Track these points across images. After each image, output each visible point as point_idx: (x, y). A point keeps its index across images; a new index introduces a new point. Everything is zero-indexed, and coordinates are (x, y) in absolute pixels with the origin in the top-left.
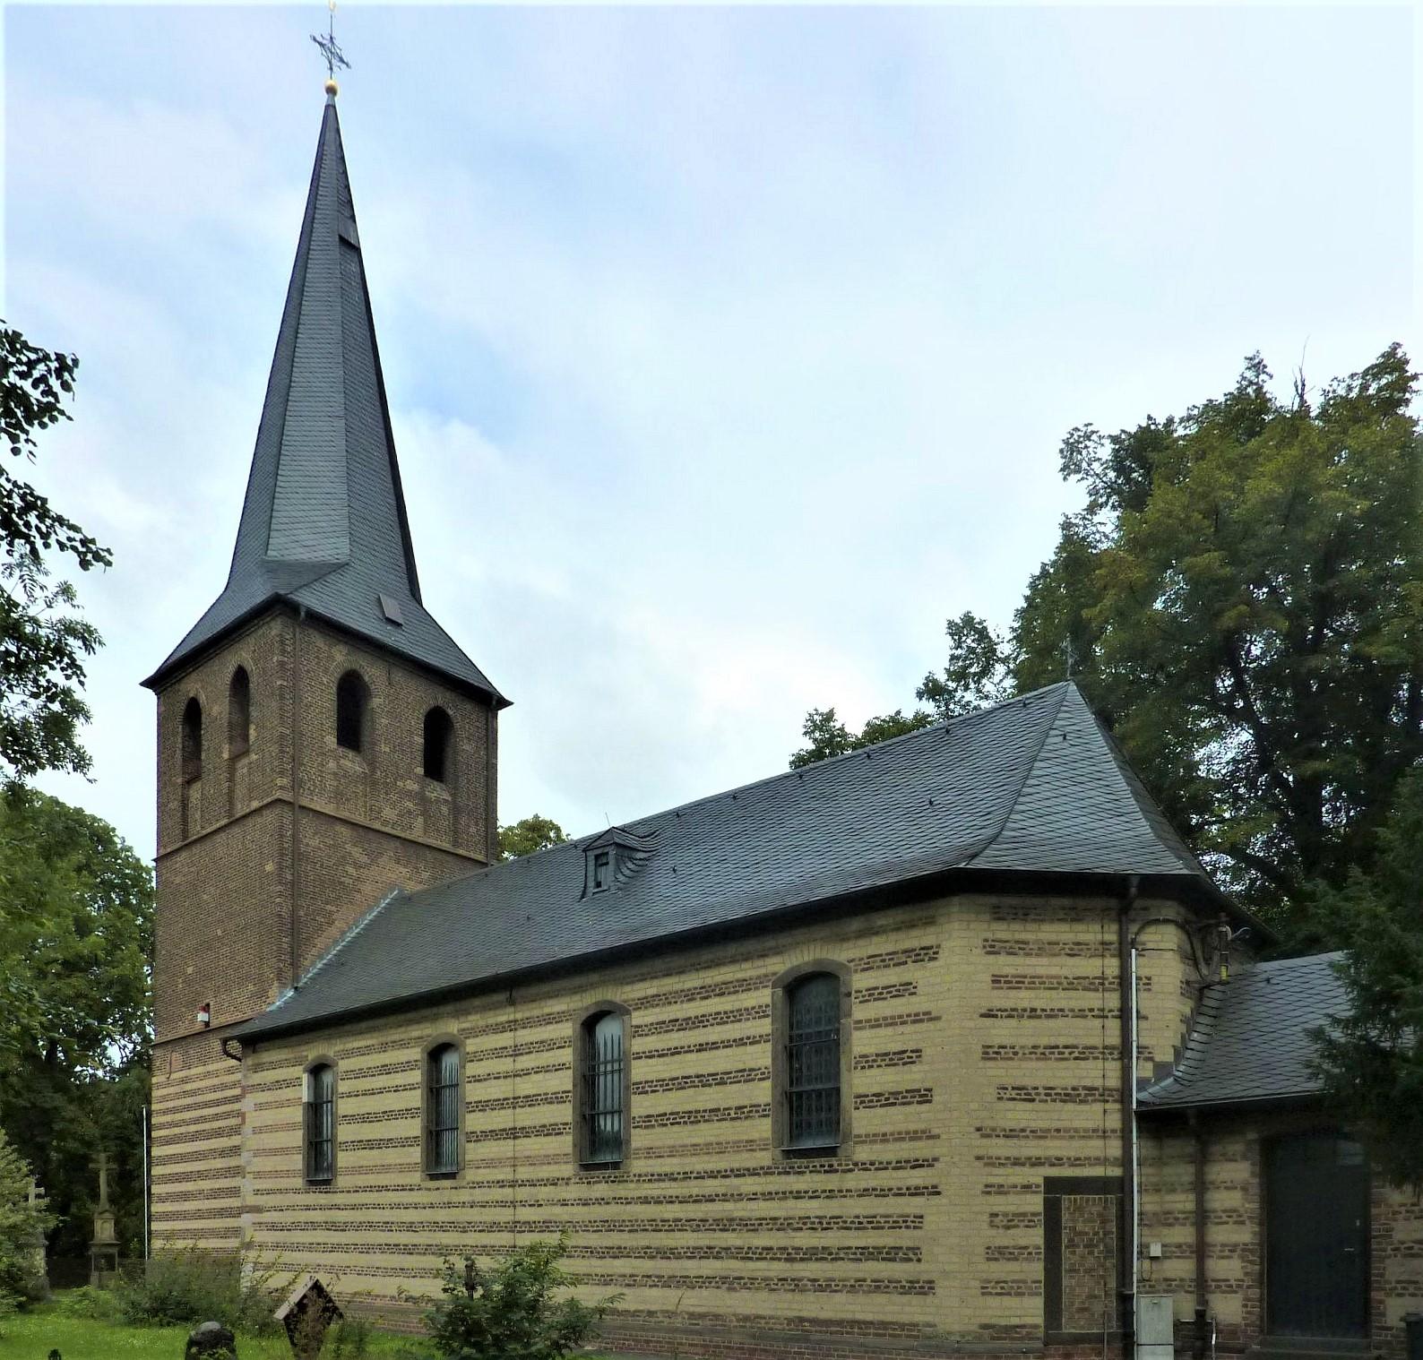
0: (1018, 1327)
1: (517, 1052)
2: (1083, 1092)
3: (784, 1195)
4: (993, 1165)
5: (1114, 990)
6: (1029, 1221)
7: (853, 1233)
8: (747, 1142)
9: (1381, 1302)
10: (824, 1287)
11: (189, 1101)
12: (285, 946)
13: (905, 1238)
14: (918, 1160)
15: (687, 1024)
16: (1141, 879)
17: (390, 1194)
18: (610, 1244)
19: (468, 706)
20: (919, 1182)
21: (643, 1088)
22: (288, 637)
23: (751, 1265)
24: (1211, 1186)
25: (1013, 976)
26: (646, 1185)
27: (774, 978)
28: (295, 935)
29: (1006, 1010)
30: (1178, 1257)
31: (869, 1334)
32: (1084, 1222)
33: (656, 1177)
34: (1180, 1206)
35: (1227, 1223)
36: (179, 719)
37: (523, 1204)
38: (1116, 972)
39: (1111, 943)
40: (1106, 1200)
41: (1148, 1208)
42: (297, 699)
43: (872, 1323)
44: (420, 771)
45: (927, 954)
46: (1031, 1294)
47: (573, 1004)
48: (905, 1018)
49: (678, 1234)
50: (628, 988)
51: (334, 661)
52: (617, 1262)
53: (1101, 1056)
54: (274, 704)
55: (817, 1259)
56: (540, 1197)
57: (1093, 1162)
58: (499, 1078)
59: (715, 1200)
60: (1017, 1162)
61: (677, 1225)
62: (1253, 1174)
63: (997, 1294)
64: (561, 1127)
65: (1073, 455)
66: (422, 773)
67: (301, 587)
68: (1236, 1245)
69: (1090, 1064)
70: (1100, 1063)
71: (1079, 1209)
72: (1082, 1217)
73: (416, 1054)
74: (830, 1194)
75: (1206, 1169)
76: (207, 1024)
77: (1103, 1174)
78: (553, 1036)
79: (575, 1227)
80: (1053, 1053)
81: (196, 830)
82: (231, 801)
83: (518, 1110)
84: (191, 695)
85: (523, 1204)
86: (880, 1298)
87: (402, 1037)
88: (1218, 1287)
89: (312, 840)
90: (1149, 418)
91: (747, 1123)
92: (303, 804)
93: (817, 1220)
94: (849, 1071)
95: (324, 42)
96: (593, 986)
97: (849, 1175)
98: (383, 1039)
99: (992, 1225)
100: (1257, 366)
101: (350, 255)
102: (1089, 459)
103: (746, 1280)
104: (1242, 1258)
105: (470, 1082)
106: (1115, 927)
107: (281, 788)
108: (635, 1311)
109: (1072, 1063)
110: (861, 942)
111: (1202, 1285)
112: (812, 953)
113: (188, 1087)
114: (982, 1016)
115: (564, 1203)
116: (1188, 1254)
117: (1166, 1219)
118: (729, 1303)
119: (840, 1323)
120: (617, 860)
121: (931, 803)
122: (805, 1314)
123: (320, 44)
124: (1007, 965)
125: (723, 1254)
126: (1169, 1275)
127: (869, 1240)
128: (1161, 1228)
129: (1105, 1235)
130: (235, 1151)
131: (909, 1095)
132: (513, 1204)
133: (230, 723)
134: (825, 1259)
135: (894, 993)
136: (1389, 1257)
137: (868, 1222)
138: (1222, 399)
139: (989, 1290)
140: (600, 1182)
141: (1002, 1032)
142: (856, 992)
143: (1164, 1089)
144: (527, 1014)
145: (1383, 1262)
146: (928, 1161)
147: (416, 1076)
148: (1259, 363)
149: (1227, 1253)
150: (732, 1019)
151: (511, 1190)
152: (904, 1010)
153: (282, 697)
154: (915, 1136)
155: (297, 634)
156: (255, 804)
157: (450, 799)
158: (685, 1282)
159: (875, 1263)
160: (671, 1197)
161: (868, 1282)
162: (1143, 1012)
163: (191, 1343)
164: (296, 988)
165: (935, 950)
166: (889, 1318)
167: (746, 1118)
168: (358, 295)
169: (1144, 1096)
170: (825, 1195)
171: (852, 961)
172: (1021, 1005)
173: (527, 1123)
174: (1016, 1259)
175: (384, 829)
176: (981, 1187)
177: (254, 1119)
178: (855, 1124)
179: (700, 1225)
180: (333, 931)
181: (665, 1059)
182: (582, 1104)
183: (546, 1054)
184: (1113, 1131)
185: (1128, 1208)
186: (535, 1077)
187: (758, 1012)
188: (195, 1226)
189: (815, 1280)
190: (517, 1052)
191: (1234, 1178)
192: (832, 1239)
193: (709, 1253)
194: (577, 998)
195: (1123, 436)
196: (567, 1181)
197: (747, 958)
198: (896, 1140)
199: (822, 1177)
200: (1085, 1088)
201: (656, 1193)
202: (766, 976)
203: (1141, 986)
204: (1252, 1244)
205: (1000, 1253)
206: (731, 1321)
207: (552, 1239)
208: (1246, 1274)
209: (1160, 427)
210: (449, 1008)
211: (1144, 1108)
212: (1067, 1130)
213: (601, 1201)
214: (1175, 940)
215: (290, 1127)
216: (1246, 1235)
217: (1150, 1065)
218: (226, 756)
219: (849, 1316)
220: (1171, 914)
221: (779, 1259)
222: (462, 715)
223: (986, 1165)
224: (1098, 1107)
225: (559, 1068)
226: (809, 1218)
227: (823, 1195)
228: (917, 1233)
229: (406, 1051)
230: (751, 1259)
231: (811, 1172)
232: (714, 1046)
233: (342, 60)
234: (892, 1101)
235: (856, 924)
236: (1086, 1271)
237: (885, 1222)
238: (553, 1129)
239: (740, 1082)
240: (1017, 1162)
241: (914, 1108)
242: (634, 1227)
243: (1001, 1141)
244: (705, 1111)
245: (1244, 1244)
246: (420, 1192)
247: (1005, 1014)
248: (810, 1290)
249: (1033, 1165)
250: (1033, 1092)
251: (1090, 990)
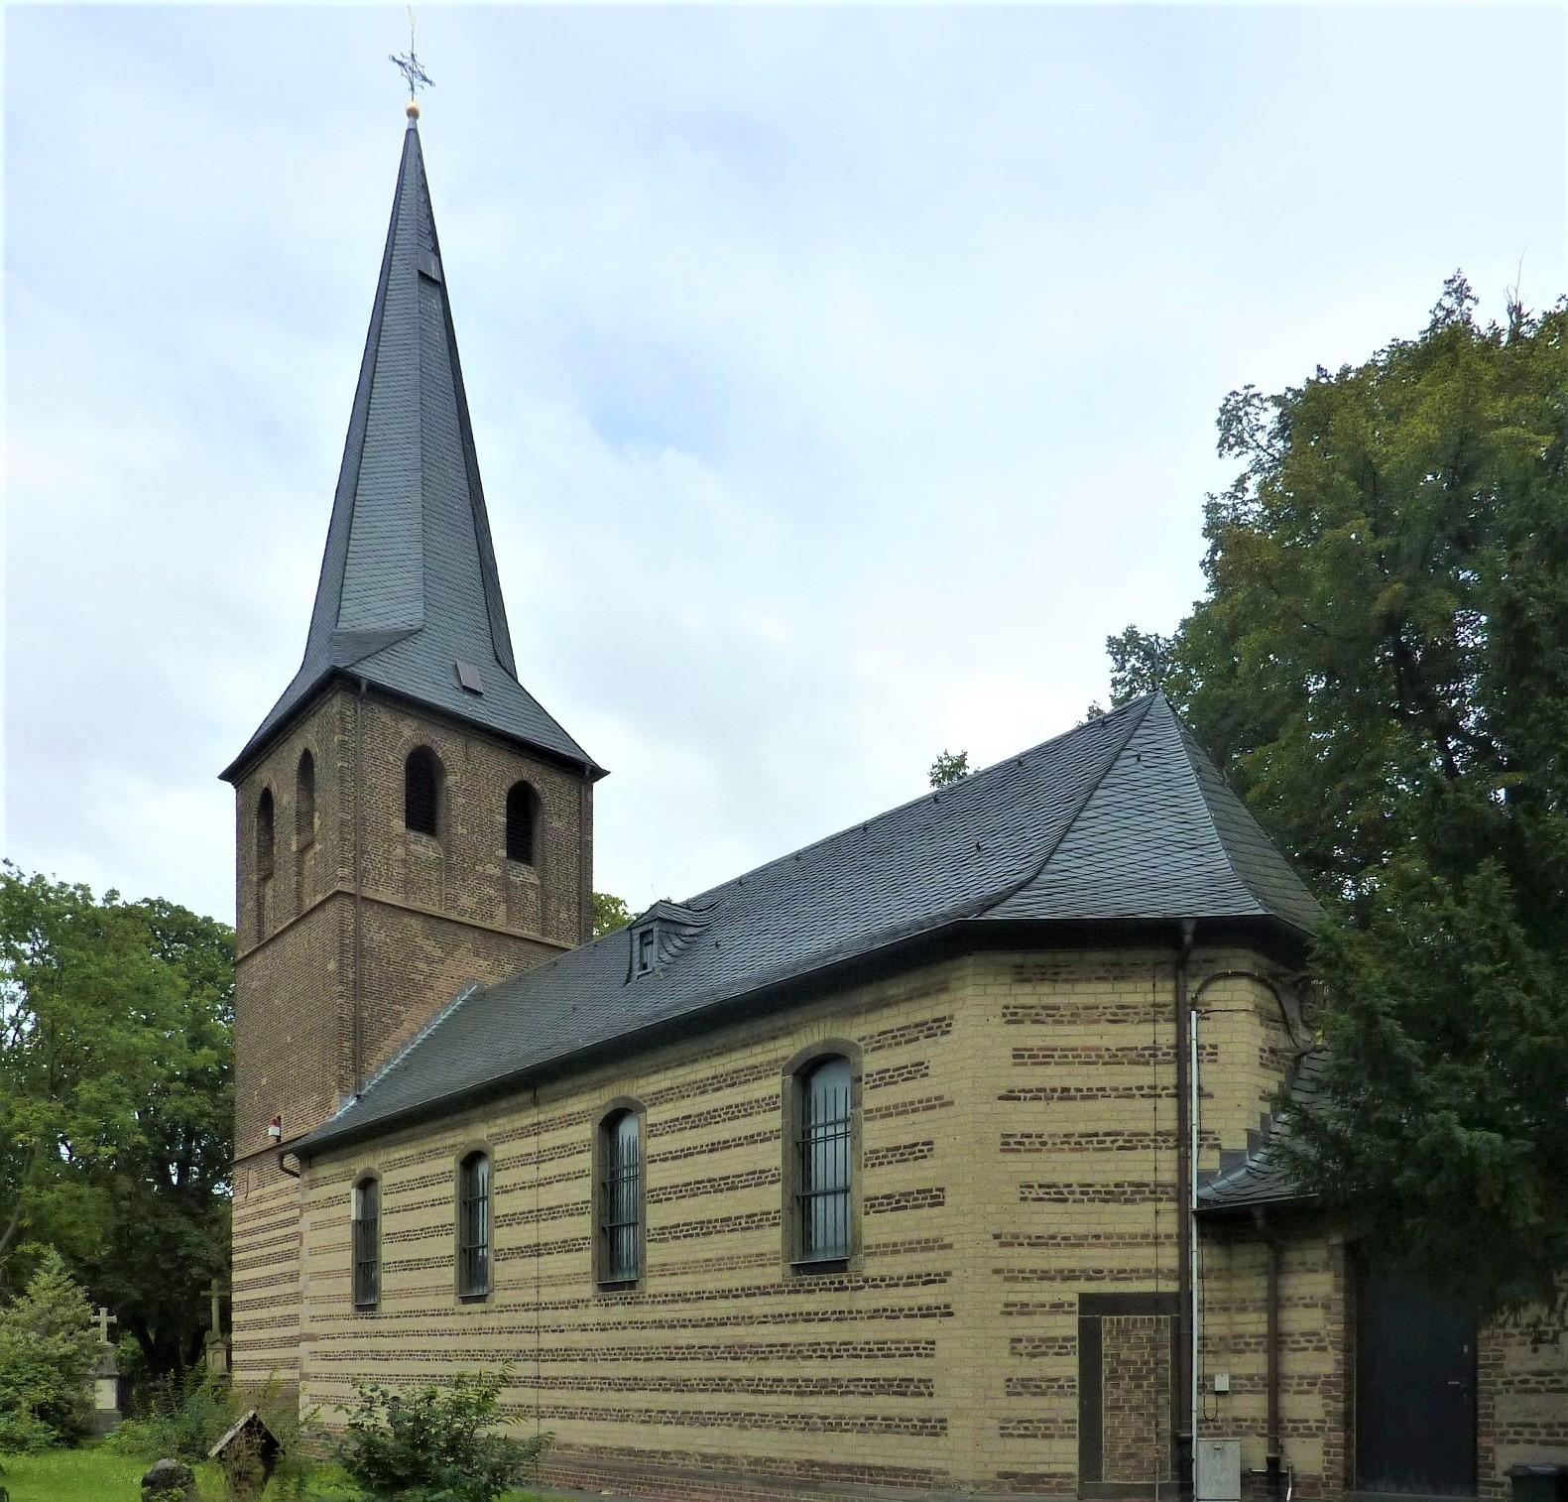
0: (1045, 1475)
1: (540, 1158)
2: (1129, 1190)
3: (794, 1318)
4: (1014, 1279)
5: (1169, 1062)
6: (1061, 1347)
7: (863, 1362)
8: (757, 1255)
9: (1490, 1450)
10: (834, 1425)
11: (263, 1221)
12: (346, 1051)
13: (912, 1368)
14: (929, 1275)
15: (700, 1120)
16: (1197, 925)
17: (428, 1319)
18: (626, 1375)
19: (558, 779)
20: (931, 1301)
21: (658, 1195)
22: (348, 713)
23: (762, 1399)
24: (1287, 1304)
25: (1041, 1049)
26: (661, 1307)
27: (784, 1063)
28: (357, 1042)
29: (1031, 1091)
30: (1251, 1392)
31: (879, 1482)
32: (1129, 1349)
33: (670, 1298)
34: (1252, 1329)
35: (1305, 1349)
36: (255, 812)
37: (547, 1329)
38: (1172, 1040)
39: (1165, 1005)
40: (1158, 1320)
41: (1211, 1331)
42: (360, 781)
43: (882, 1469)
44: (503, 853)
45: (938, 1027)
46: (1062, 1437)
47: (591, 1101)
48: (917, 1105)
49: (690, 1363)
50: (643, 1082)
51: (402, 736)
52: (634, 1395)
53: (1152, 1145)
54: (335, 787)
55: (827, 1393)
56: (562, 1321)
57: (1142, 1274)
58: (524, 1188)
59: (726, 1324)
60: (1045, 1276)
61: (689, 1353)
62: (1336, 1289)
63: (1019, 1436)
64: (581, 1242)
65: (1231, 423)
66: (505, 854)
67: (364, 659)
68: (1316, 1377)
69: (1139, 1154)
70: (1150, 1154)
71: (1124, 1332)
72: (1130, 1344)
73: (449, 1164)
74: (840, 1316)
75: (1281, 1282)
76: (278, 1138)
77: (1153, 1290)
78: (574, 1139)
79: (593, 1355)
80: (1091, 1142)
81: (270, 931)
82: (299, 898)
83: (542, 1224)
84: (265, 785)
85: (547, 1329)
86: (891, 1439)
87: (439, 1145)
88: (1296, 1429)
89: (377, 933)
90: (1319, 369)
91: (758, 1233)
92: (367, 895)
93: (827, 1347)
94: (859, 1169)
95: (404, 61)
96: (610, 1081)
97: (860, 1293)
98: (421, 1149)
99: (1014, 1352)
100: (1459, 290)
101: (431, 291)
102: (1251, 428)
103: (757, 1417)
104: (1325, 1395)
105: (498, 1193)
106: (1170, 985)
107: (342, 879)
108: (650, 1452)
109: (1115, 1154)
110: (872, 1017)
111: (1275, 1426)
112: (822, 1034)
113: (264, 1206)
114: (1001, 1098)
115: (584, 1328)
116: (1261, 1388)
117: (1234, 1345)
118: (741, 1443)
119: (850, 1468)
120: (661, 938)
121: (979, 848)
122: (815, 1457)
123: (400, 63)
124: (1033, 1036)
125: (735, 1386)
126: (1240, 1414)
127: (879, 1370)
128: (1230, 1356)
129: (1156, 1364)
130: (293, 1277)
131: (920, 1196)
132: (537, 1330)
133: (298, 813)
134: (835, 1393)
135: (906, 1075)
136: (1500, 1393)
137: (878, 1349)
138: (1417, 339)
139: (1010, 1431)
140: (617, 1304)
141: (1027, 1117)
142: (867, 1076)
143: (1232, 1183)
144: (550, 1116)
145: (1491, 1399)
146: (940, 1275)
147: (450, 1189)
148: (1461, 285)
149: (1305, 1387)
150: (743, 1113)
151: (535, 1313)
152: (915, 1096)
153: (342, 780)
154: (926, 1245)
155: (359, 710)
156: (320, 898)
157: (538, 882)
158: (697, 1418)
159: (886, 1397)
160: (684, 1320)
161: (879, 1421)
162: (1207, 1089)
163: (146, 1482)
164: (358, 1096)
165: (947, 1022)
166: (899, 1464)
167: (757, 1227)
168: (439, 334)
169: (1207, 1192)
170: (835, 1316)
171: (863, 1039)
172: (1049, 1084)
173: (551, 1239)
174: (1043, 1394)
175: (460, 919)
176: (1000, 1307)
177: (312, 1239)
178: (865, 1231)
179: (711, 1352)
180: (402, 1034)
181: (679, 1161)
182: (600, 1216)
183: (566, 1160)
184: (1168, 1236)
185: (1185, 1331)
186: (556, 1186)
187: (768, 1104)
188: (268, 1356)
189: (825, 1418)
190: (540, 1158)
191: (1315, 1290)
192: (842, 1369)
193: (721, 1385)
194: (596, 1094)
195: (1290, 396)
196: (585, 1302)
197: (757, 1040)
198: (906, 1251)
199: (832, 1296)
200: (1131, 1184)
201: (670, 1316)
202: (776, 1061)
203: (1205, 1058)
204: (1335, 1376)
205: (1023, 1386)
206: (743, 1464)
207: (497, 1368)
208: (1328, 1413)
209: (1332, 380)
210: (479, 1112)
211: (1205, 1208)
212: (1108, 1237)
213: (618, 1326)
214: (1252, 998)
215: (340, 1247)
216: (1327, 1364)
217: (1215, 1154)
218: (294, 848)
219: (859, 1461)
220: (1244, 966)
221: (790, 1393)
222: (549, 786)
223: (1006, 1279)
224: (1149, 1207)
225: (579, 1175)
226: (819, 1344)
227: (834, 1317)
228: (928, 1362)
229: (441, 1161)
230: (761, 1392)
231: (821, 1290)
232: (725, 1145)
233: (425, 79)
234: (903, 1203)
235: (867, 995)
236: (1132, 1409)
237: (896, 1349)
238: (574, 1245)
239: (751, 1185)
240: (1045, 1276)
241: (926, 1212)
242: (648, 1356)
243: (1025, 1251)
244: (716, 1221)
245: (1326, 1376)
246: (454, 1317)
247: (1029, 1095)
248: (819, 1429)
249: (1066, 1279)
250: (1065, 1190)
251: (1138, 1063)
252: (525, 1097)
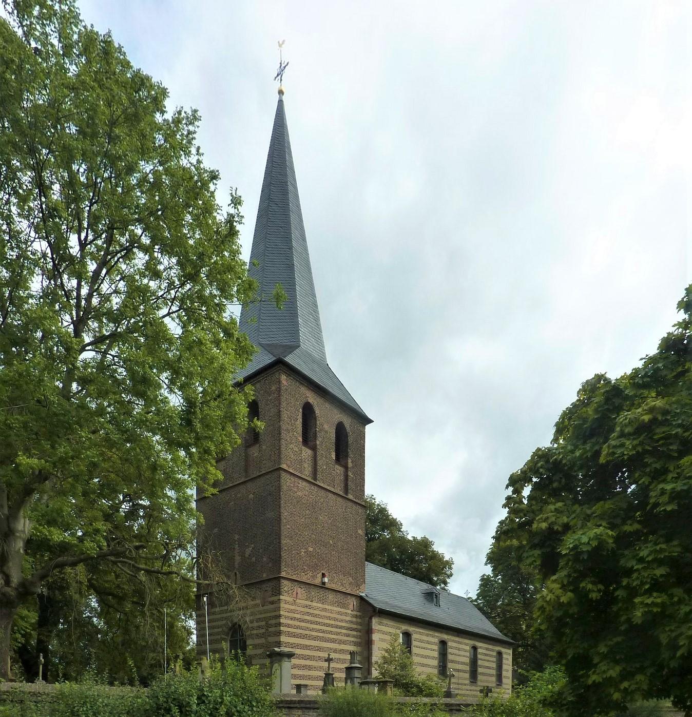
252: (456, 634)
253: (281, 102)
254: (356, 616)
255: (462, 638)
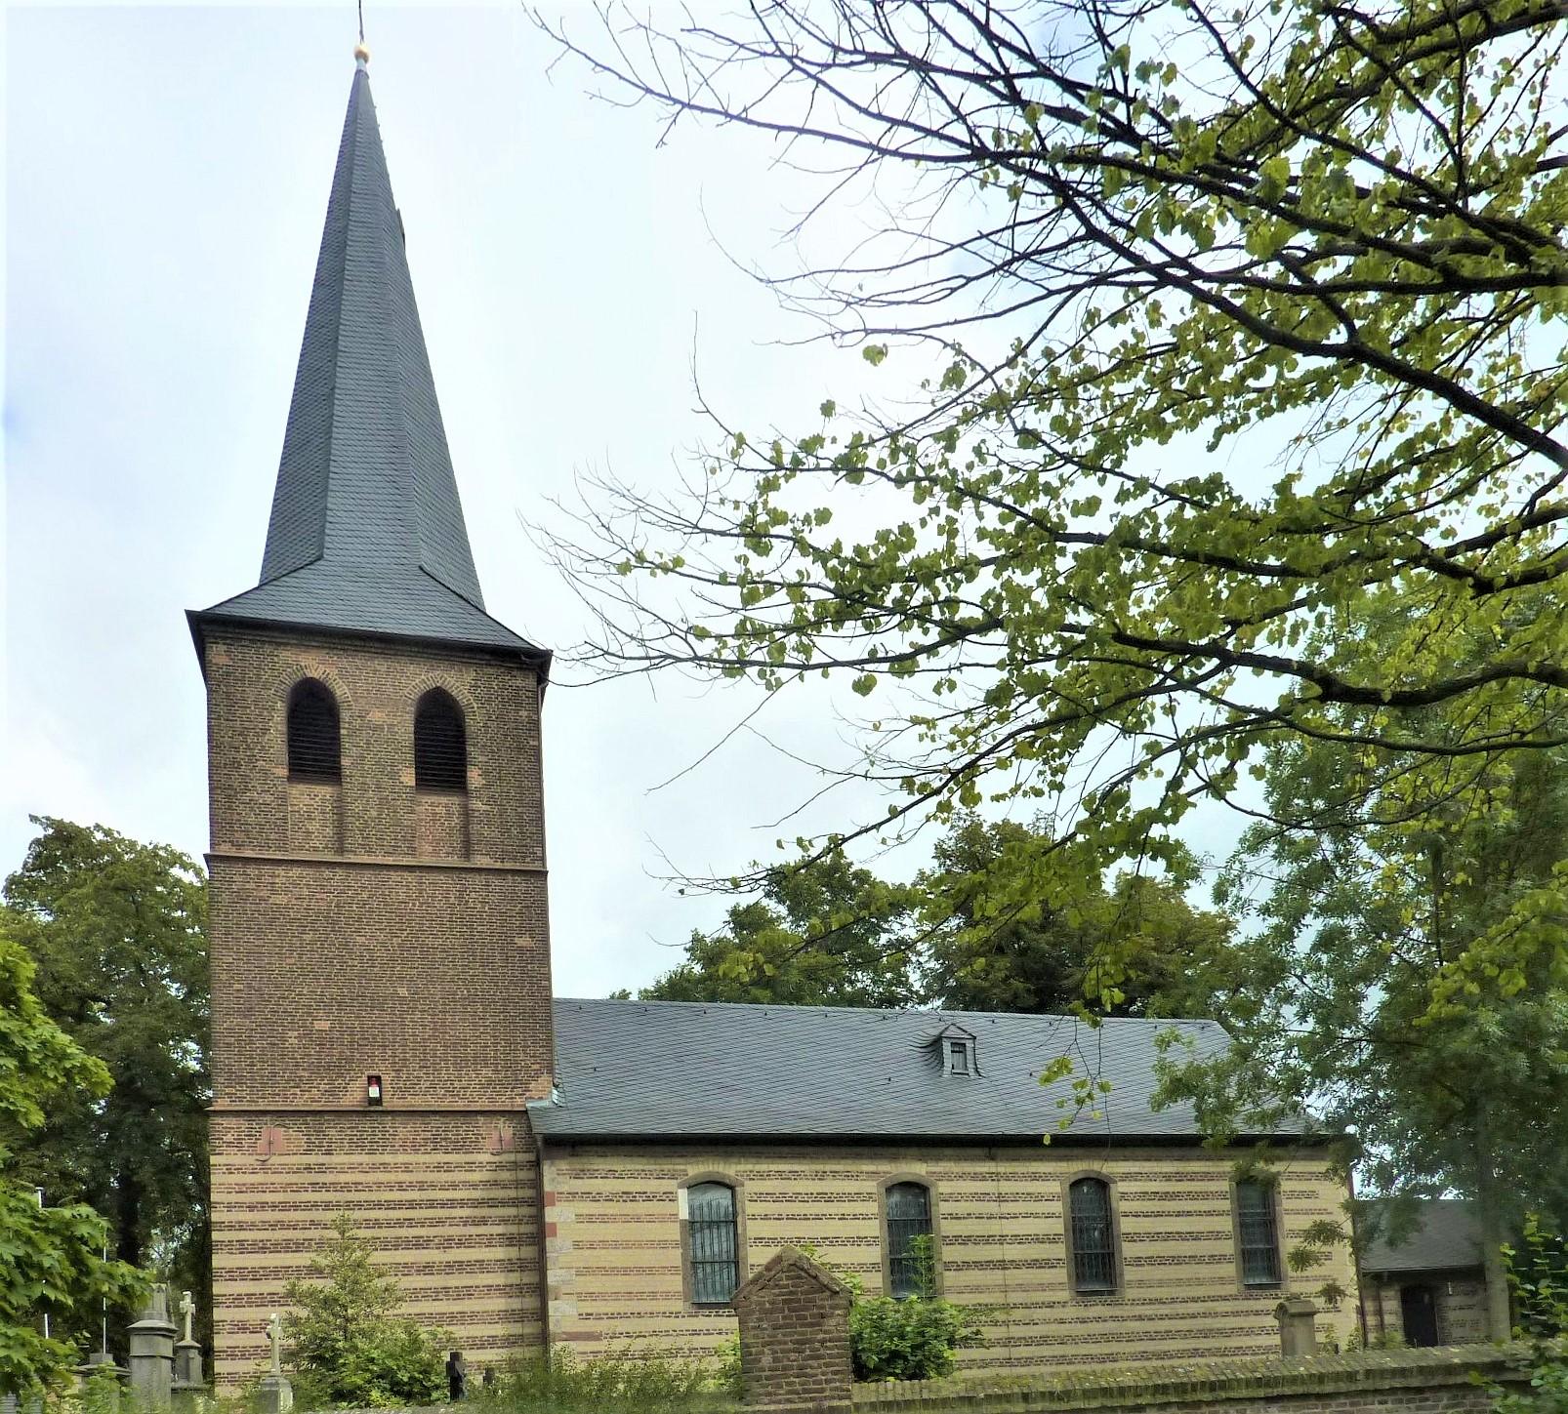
179: (1187, 1334)
196: (1064, 1304)
232: (1189, 1214)
252: (569, 1150)
253: (360, 78)
254: (515, 1166)
255: (615, 1160)
